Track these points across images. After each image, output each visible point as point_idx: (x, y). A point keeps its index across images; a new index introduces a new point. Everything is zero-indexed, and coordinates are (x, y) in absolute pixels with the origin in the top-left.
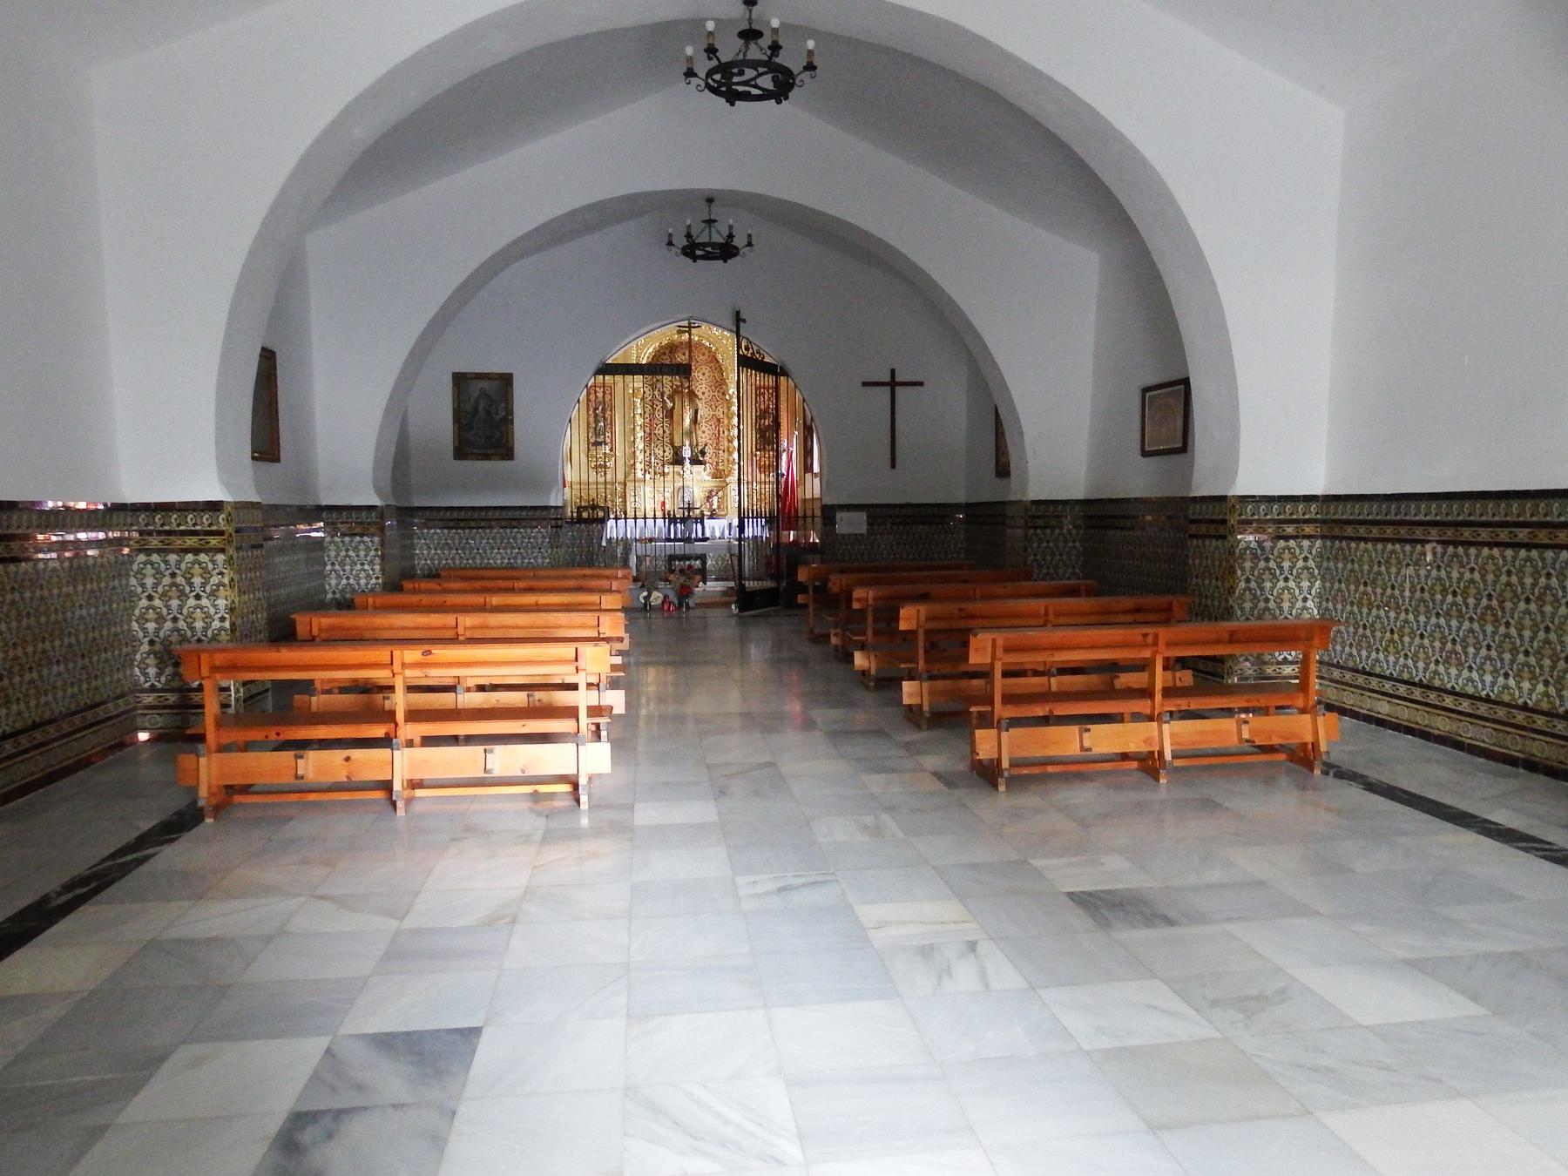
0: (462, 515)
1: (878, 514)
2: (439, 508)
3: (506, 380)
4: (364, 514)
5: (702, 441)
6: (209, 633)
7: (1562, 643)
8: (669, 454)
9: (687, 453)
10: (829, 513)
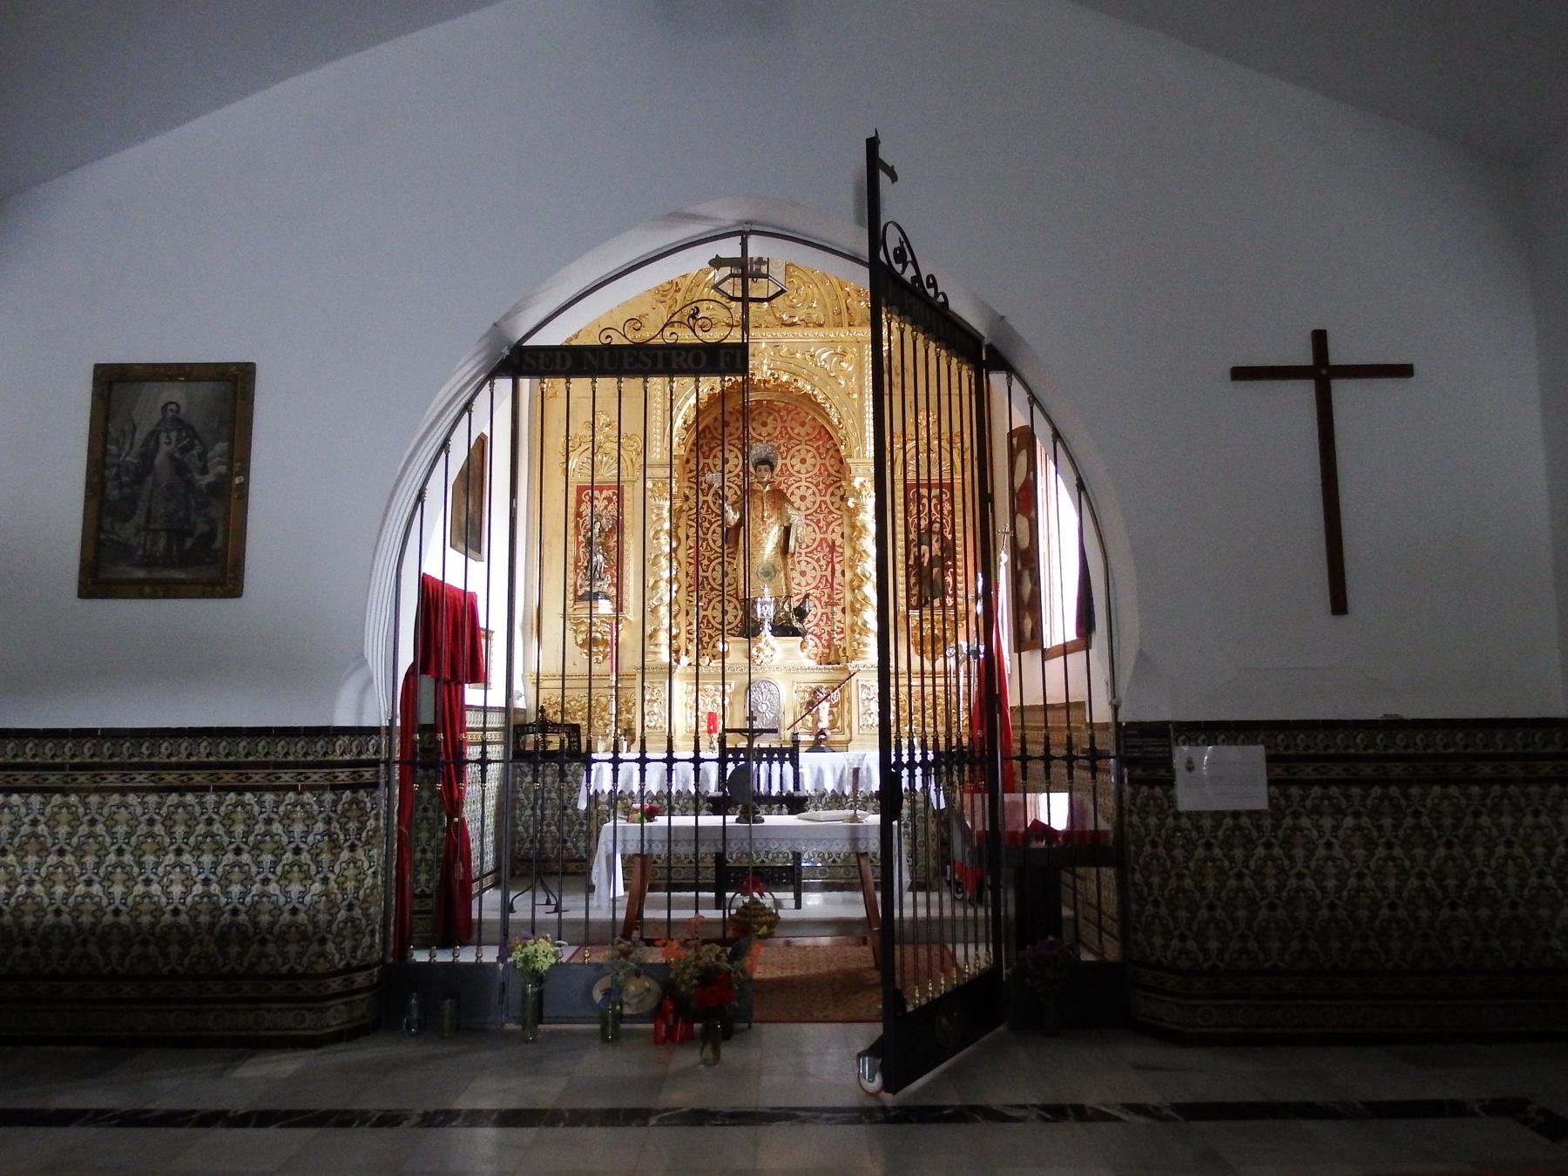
0: (87, 752)
1: (1303, 753)
2: (90, 733)
3: (234, 385)
4: (69, 746)
5: (798, 591)
6: (130, 900)
7: (1559, 826)
8: (734, 615)
9: (765, 611)
10: (1144, 750)
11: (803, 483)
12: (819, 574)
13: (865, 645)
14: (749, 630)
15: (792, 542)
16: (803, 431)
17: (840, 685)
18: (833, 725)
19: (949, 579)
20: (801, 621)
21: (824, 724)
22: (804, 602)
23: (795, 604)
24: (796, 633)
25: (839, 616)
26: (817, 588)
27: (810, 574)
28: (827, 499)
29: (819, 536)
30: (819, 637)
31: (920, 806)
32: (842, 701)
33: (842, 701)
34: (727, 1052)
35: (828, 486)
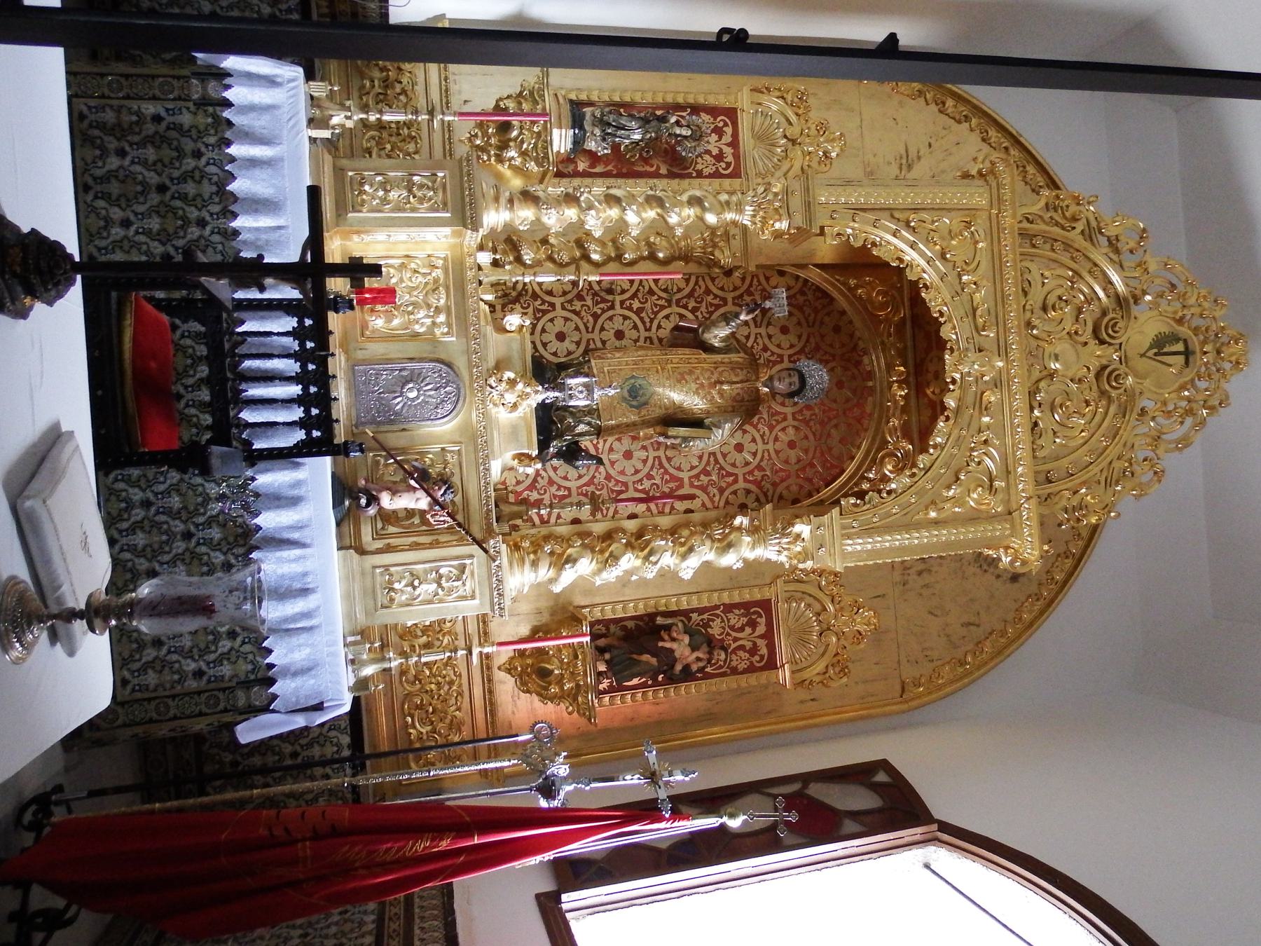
9: (577, 392)
11: (761, 447)
12: (630, 479)
13: (535, 564)
14: (544, 371)
15: (683, 431)
16: (834, 442)
17: (463, 528)
18: (388, 517)
19: (635, 681)
20: (559, 455)
21: (386, 501)
22: (591, 457)
23: (586, 443)
24: (543, 445)
25: (568, 513)
26: (608, 477)
27: (629, 466)
28: (741, 484)
29: (685, 476)
30: (532, 487)
31: (241, 699)
32: (432, 531)
33: (432, 531)
34: (552, 603)
35: (758, 483)
